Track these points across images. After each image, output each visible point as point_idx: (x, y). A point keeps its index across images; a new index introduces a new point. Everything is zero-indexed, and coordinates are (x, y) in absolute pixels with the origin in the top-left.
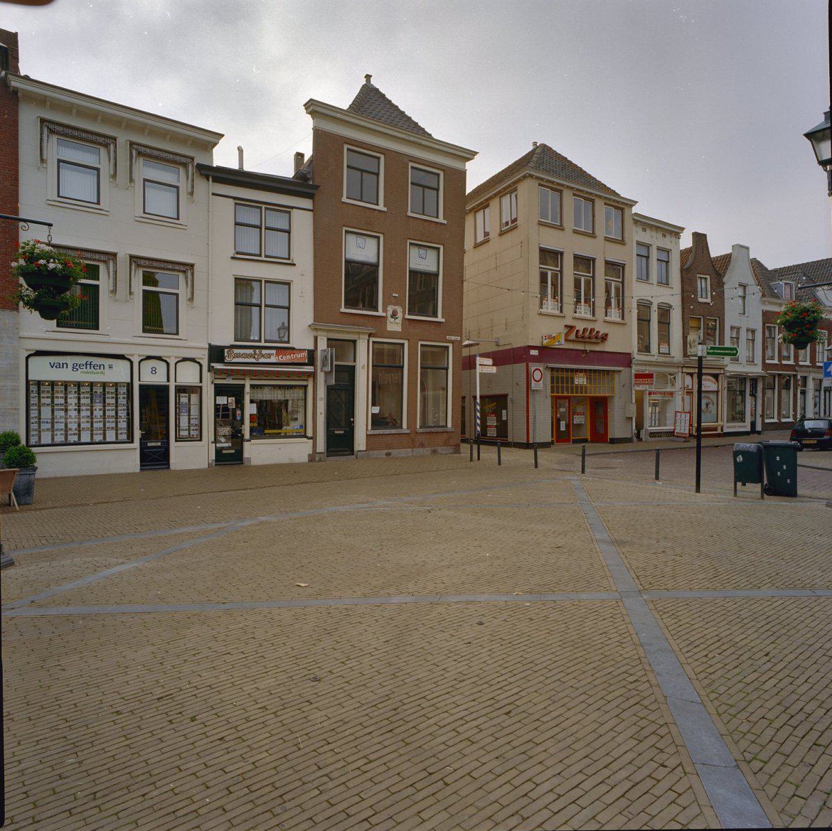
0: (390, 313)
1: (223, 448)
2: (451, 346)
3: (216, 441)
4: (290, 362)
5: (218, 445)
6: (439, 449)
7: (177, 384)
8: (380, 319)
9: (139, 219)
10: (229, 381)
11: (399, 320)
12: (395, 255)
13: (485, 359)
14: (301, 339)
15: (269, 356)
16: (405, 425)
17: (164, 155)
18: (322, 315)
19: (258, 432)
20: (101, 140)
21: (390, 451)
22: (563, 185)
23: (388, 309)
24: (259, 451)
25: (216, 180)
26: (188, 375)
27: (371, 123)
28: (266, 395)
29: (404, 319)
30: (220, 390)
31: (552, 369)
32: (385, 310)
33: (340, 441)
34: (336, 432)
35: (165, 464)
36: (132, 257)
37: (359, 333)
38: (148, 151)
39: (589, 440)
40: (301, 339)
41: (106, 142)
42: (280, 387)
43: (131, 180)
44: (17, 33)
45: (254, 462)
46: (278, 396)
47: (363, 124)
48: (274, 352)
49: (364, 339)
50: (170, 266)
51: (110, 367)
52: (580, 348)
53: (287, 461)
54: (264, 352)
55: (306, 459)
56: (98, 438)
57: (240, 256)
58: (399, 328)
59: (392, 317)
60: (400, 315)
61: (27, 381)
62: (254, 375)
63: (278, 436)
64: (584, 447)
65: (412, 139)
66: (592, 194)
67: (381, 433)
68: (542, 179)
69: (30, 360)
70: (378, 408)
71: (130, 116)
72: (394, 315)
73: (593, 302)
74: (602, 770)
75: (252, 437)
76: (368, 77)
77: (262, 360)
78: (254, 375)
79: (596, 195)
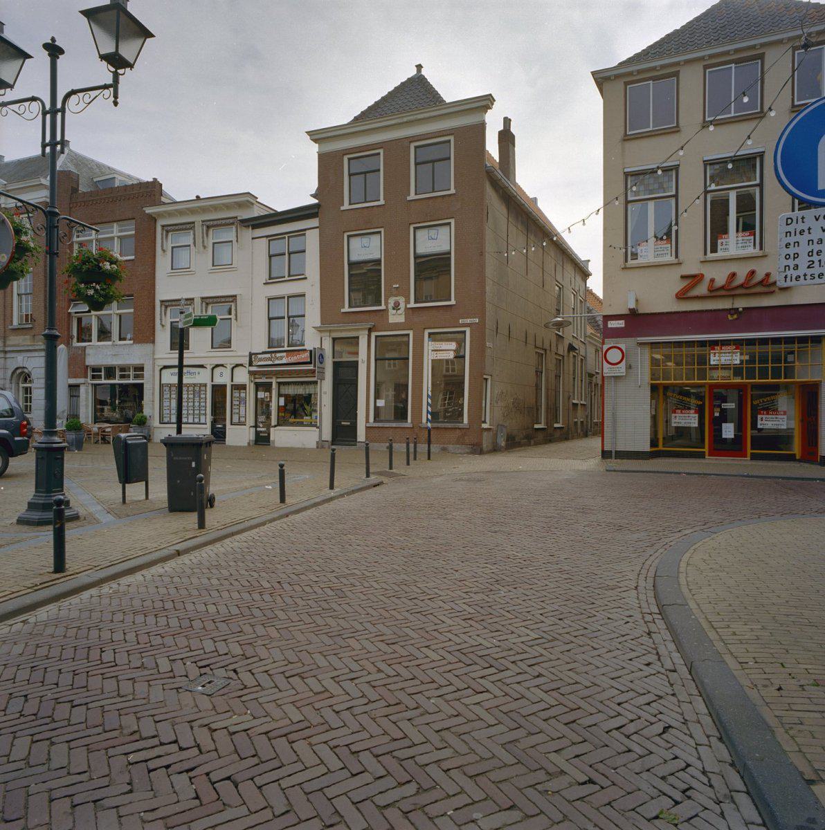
0: (391, 305)
1: (261, 432)
2: (468, 330)
3: (256, 426)
4: (297, 361)
5: (258, 429)
6: (451, 447)
7: (213, 383)
8: (382, 313)
9: (212, 271)
10: (264, 380)
11: (401, 311)
12: (397, 244)
13: (443, 343)
14: (311, 342)
15: (281, 358)
16: (466, 420)
17: (219, 222)
18: (329, 314)
19: (282, 422)
20: (188, 226)
21: (445, 446)
22: (678, 64)
23: (389, 301)
24: (283, 436)
25: (254, 227)
26: (242, 377)
27: (366, 124)
28: (291, 391)
29: (406, 309)
30: (258, 386)
31: (653, 345)
32: (386, 304)
33: (343, 432)
34: (343, 423)
35: (353, 441)
36: (203, 298)
37: (358, 330)
38: (215, 223)
39: (798, 457)
40: (311, 342)
41: (190, 226)
42: (302, 383)
43: (205, 247)
44: (155, 179)
45: (278, 444)
46: (300, 390)
47: (419, 117)
48: (284, 354)
49: (363, 334)
50: (223, 300)
51: (199, 374)
52: (727, 307)
53: (300, 446)
54: (278, 355)
55: (246, 445)
56: (196, 420)
57: (272, 280)
58: (401, 319)
59: (394, 309)
60: (402, 306)
61: (161, 386)
62: (277, 374)
63: (301, 424)
64: (333, 450)
65: (405, 119)
66: (753, 47)
67: (380, 426)
68: (702, 59)
69: (235, 370)
70: (383, 401)
71: (211, 203)
72: (396, 307)
73: (677, 231)
74: (56, 787)
75: (278, 425)
76: (419, 67)
77: (277, 362)
78: (277, 374)
79: (763, 45)
